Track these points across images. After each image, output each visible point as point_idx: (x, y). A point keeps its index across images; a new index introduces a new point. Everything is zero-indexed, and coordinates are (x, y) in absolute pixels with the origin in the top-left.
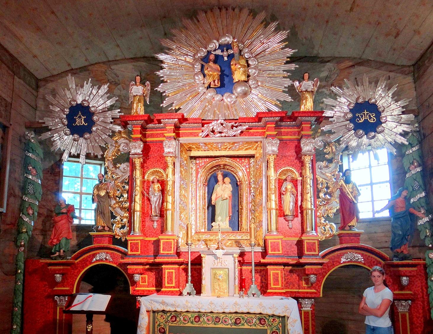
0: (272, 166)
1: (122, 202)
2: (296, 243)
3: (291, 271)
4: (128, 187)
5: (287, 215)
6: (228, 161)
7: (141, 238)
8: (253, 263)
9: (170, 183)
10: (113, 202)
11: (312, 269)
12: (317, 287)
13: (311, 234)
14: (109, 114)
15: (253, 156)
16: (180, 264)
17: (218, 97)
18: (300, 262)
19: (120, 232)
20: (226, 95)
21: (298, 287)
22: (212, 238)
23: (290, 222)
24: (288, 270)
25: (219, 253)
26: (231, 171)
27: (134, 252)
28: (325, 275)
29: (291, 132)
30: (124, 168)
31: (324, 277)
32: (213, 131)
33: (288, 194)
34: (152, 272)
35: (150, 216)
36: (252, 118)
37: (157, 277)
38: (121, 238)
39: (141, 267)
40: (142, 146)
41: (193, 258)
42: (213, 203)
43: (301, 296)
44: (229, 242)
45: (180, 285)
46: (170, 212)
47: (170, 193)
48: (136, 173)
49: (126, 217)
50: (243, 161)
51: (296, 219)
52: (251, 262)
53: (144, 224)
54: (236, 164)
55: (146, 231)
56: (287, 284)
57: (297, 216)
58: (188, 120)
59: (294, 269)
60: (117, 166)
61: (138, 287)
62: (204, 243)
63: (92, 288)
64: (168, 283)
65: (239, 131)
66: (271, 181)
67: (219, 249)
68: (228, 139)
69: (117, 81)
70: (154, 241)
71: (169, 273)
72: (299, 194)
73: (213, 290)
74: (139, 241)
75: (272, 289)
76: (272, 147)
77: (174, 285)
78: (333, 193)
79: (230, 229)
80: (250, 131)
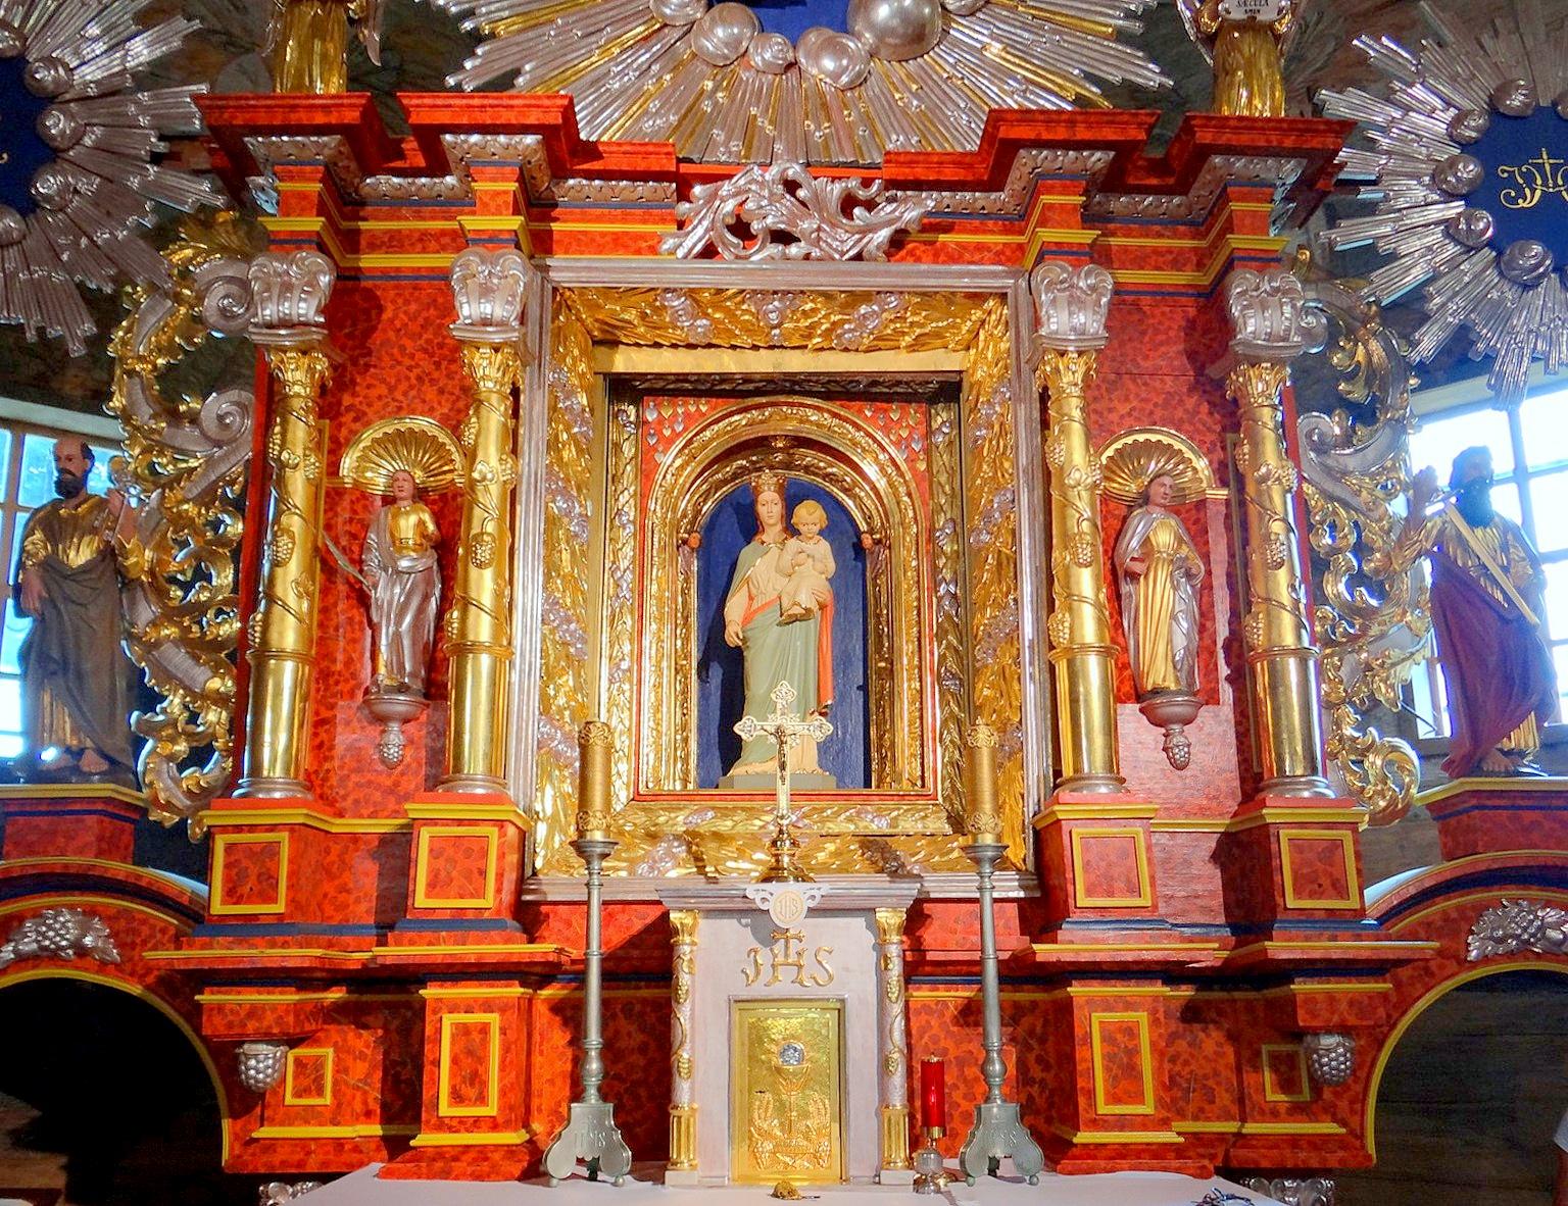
0: (1077, 414)
1: (199, 609)
2: (1211, 844)
3: (1191, 1014)
4: (240, 526)
5: (1157, 691)
6: (813, 418)
7: (297, 816)
8: (991, 969)
9: (490, 498)
10: (146, 612)
11: (1331, 998)
12: (1343, 1104)
13: (1306, 794)
14: (141, 109)
15: (948, 390)
16: (535, 975)
17: (770, 51)
18: (1271, 954)
19: (177, 782)
20: (812, 37)
21: (1235, 1110)
22: (725, 826)
23: (1176, 727)
24: (952, 1010)
25: (786, 901)
26: (825, 477)
27: (249, 901)
28: (1386, 1036)
29: (1156, 251)
30: (221, 418)
31: (1380, 1045)
32: (741, 228)
33: (1162, 574)
34: (365, 1027)
35: (367, 692)
36: (961, 160)
37: (394, 1056)
38: (183, 821)
39: (291, 997)
40: (325, 280)
41: (618, 938)
42: (732, 636)
43: (1265, 1164)
44: (831, 847)
45: (535, 1102)
46: (485, 660)
47: (484, 553)
48: (284, 434)
49: (220, 699)
50: (895, 416)
51: (1205, 713)
52: (980, 963)
53: (323, 736)
54: (859, 435)
55: (334, 781)
56: (1177, 1096)
57: (1212, 698)
58: (598, 156)
59: (1208, 1002)
60: (183, 408)
61: (272, 1122)
62: (681, 851)
63: (34, 1122)
64: (457, 1098)
65: (884, 234)
66: (1072, 494)
67: (781, 879)
68: (825, 273)
69: (237, 31)
70: (385, 840)
71: (463, 1030)
72: (1219, 580)
73: (741, 1127)
74: (284, 837)
75: (1098, 1123)
76: (1074, 315)
77: (491, 1110)
78: (1393, 577)
79: (829, 783)
80: (942, 237)
